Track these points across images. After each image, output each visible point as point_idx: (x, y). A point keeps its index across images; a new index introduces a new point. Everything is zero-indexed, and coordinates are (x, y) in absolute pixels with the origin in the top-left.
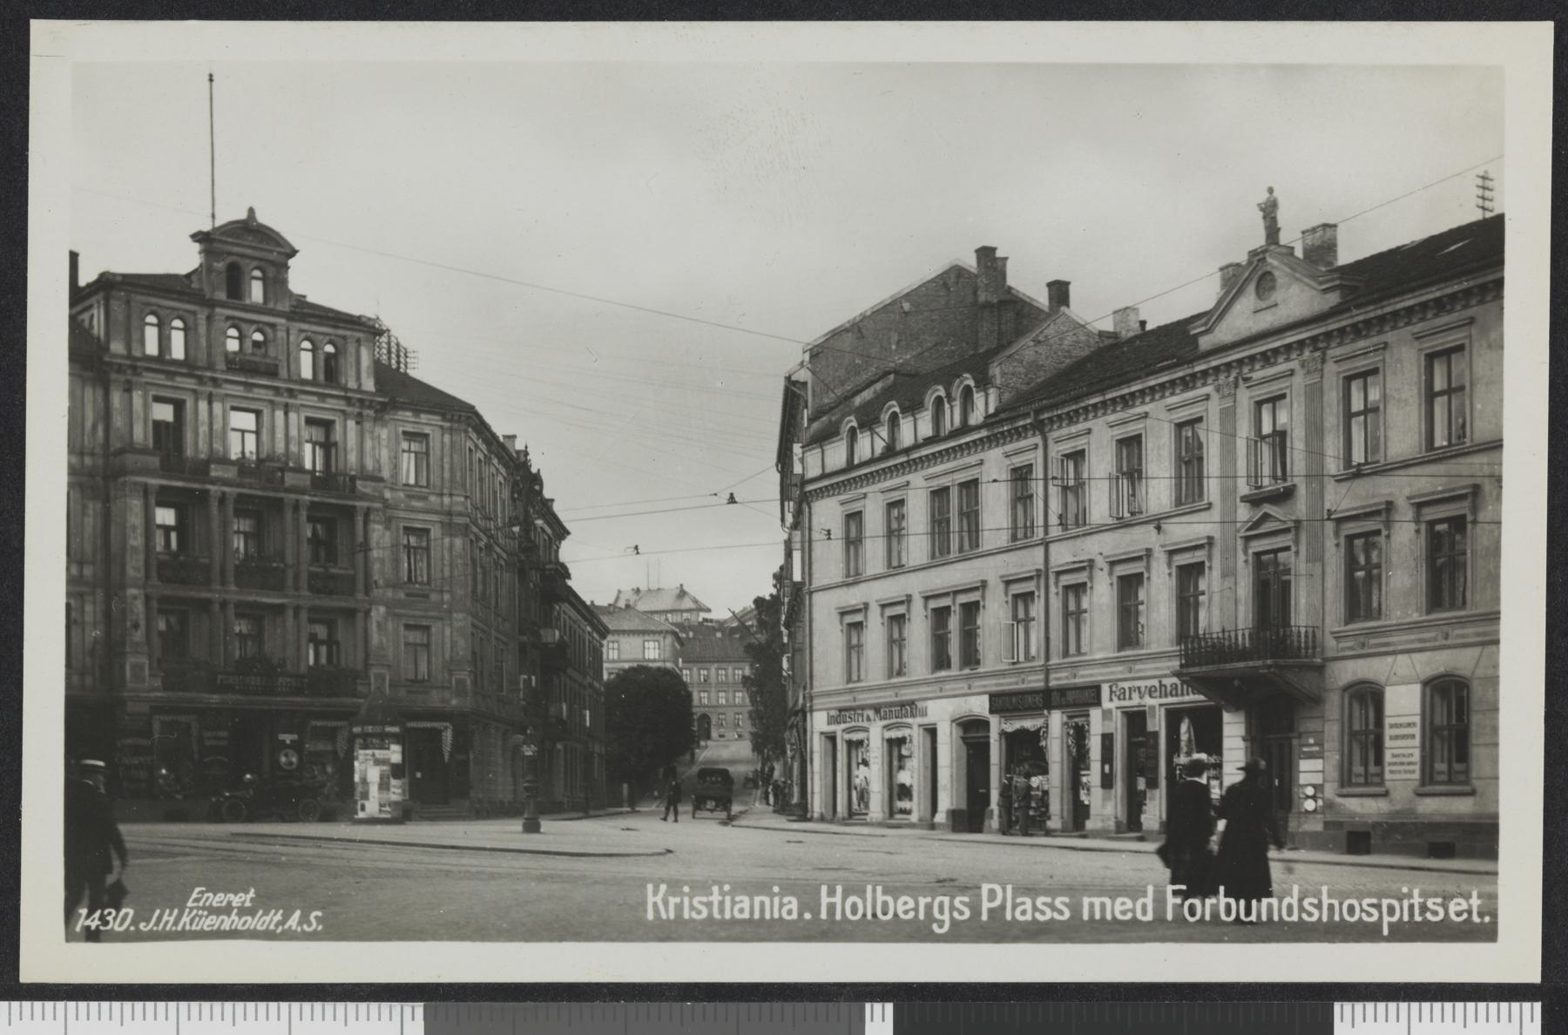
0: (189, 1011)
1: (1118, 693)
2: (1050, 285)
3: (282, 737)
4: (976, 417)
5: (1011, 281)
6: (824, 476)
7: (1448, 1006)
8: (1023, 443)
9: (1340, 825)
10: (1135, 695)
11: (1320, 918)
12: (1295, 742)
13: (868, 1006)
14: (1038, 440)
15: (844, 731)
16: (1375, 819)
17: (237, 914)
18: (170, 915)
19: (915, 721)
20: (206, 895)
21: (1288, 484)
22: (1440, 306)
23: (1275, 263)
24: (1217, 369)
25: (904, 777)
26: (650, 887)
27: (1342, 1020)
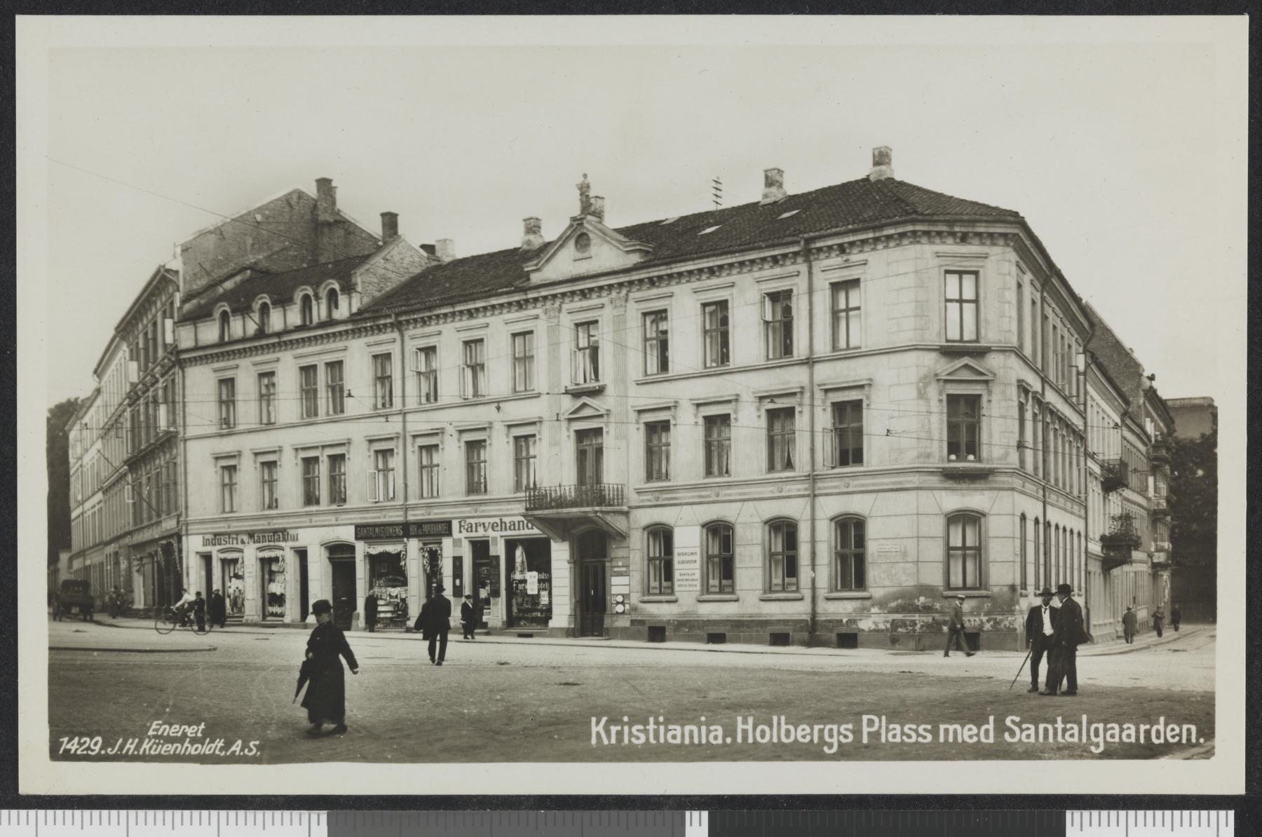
1: (466, 527)
2: (383, 215)
4: (342, 312)
5: (340, 205)
6: (196, 349)
7: (1159, 813)
8: (382, 337)
9: (642, 622)
10: (481, 529)
12: (608, 564)
13: (688, 813)
14: (396, 335)
15: (219, 551)
16: (668, 618)
17: (189, 742)
18: (129, 749)
19: (287, 545)
20: (163, 727)
21: (601, 383)
22: (712, 271)
23: (591, 228)
24: (545, 298)
25: (275, 588)
26: (594, 720)
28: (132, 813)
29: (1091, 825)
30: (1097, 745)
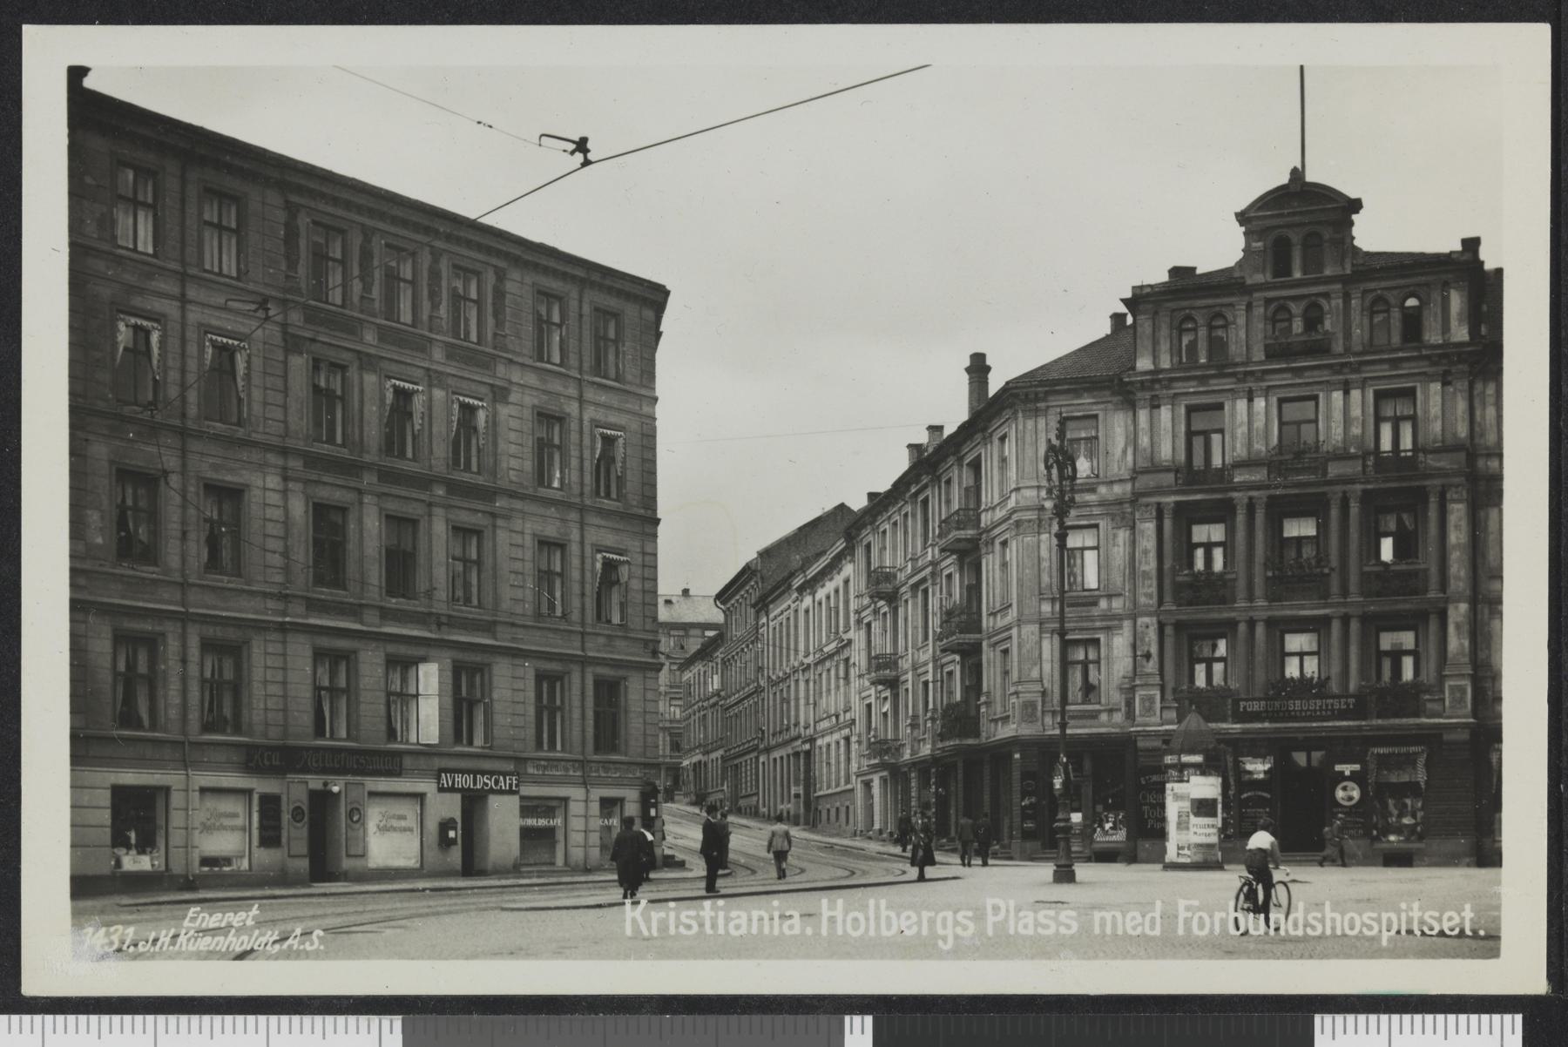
0: (167, 1024)
3: (1338, 768)
7: (1429, 1018)
11: (1323, 932)
13: (847, 1018)
20: (202, 915)
27: (1322, 1033)
28: (161, 1018)
29: (1345, 1032)
30: (944, 939)
